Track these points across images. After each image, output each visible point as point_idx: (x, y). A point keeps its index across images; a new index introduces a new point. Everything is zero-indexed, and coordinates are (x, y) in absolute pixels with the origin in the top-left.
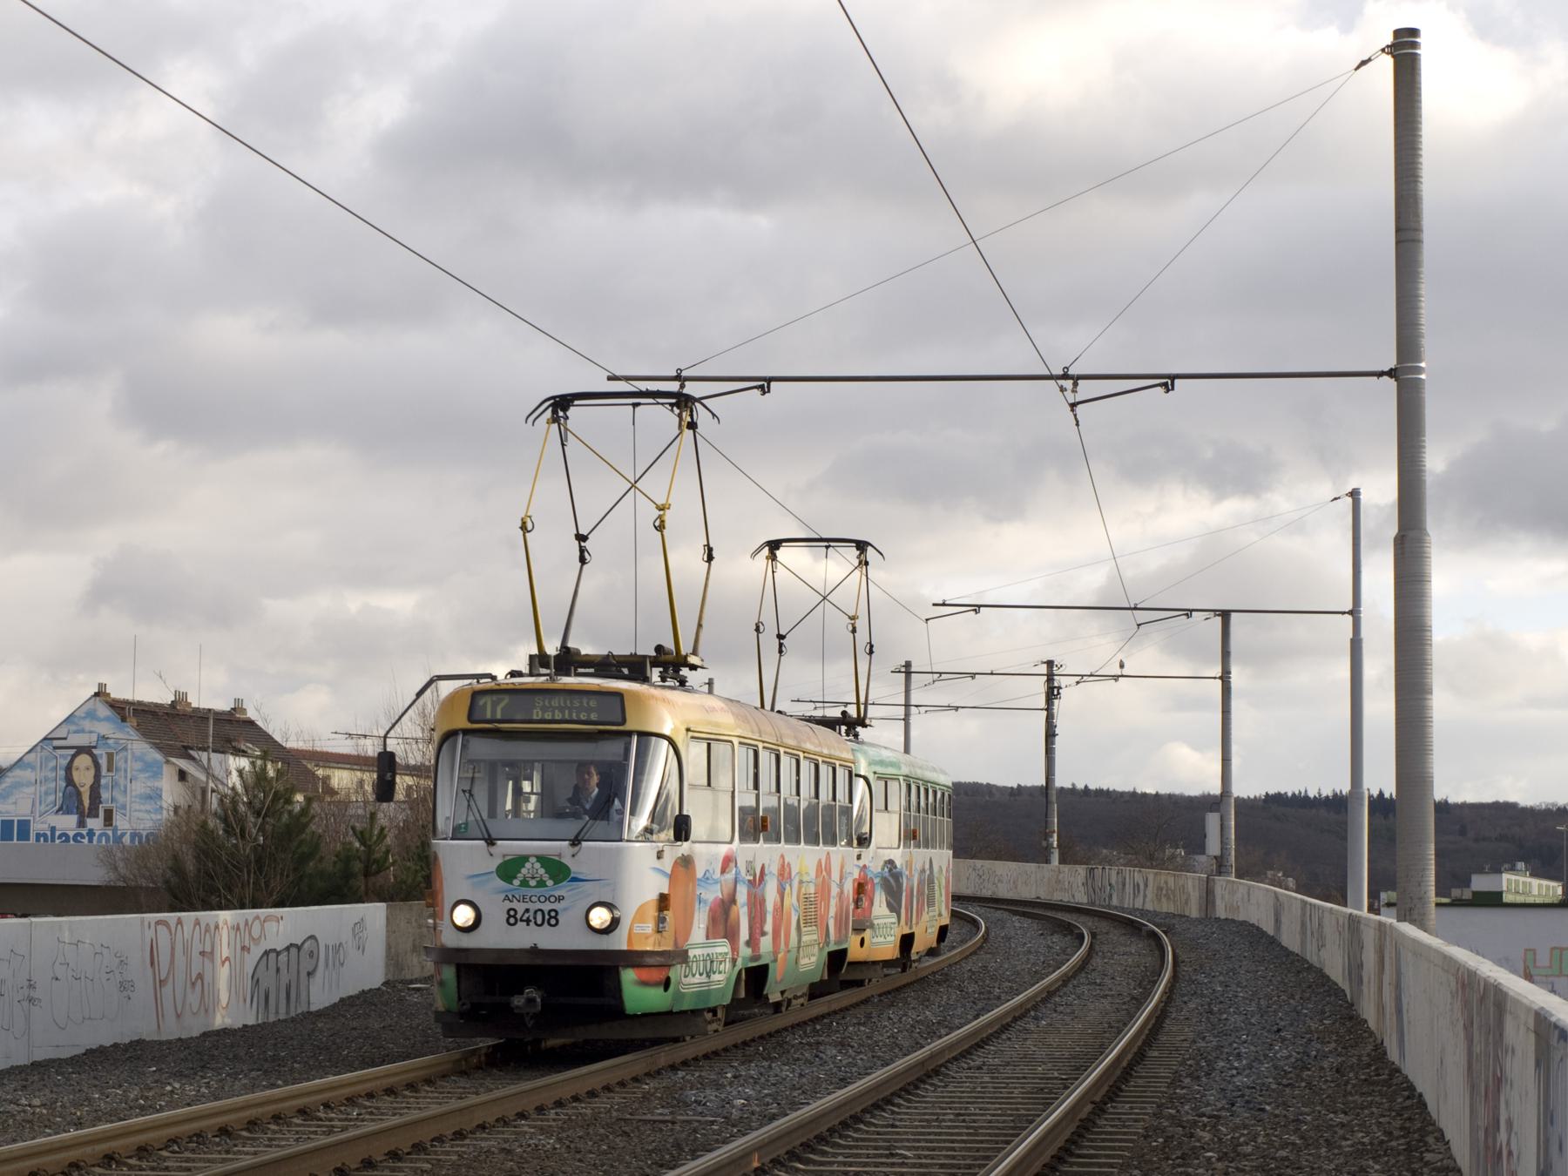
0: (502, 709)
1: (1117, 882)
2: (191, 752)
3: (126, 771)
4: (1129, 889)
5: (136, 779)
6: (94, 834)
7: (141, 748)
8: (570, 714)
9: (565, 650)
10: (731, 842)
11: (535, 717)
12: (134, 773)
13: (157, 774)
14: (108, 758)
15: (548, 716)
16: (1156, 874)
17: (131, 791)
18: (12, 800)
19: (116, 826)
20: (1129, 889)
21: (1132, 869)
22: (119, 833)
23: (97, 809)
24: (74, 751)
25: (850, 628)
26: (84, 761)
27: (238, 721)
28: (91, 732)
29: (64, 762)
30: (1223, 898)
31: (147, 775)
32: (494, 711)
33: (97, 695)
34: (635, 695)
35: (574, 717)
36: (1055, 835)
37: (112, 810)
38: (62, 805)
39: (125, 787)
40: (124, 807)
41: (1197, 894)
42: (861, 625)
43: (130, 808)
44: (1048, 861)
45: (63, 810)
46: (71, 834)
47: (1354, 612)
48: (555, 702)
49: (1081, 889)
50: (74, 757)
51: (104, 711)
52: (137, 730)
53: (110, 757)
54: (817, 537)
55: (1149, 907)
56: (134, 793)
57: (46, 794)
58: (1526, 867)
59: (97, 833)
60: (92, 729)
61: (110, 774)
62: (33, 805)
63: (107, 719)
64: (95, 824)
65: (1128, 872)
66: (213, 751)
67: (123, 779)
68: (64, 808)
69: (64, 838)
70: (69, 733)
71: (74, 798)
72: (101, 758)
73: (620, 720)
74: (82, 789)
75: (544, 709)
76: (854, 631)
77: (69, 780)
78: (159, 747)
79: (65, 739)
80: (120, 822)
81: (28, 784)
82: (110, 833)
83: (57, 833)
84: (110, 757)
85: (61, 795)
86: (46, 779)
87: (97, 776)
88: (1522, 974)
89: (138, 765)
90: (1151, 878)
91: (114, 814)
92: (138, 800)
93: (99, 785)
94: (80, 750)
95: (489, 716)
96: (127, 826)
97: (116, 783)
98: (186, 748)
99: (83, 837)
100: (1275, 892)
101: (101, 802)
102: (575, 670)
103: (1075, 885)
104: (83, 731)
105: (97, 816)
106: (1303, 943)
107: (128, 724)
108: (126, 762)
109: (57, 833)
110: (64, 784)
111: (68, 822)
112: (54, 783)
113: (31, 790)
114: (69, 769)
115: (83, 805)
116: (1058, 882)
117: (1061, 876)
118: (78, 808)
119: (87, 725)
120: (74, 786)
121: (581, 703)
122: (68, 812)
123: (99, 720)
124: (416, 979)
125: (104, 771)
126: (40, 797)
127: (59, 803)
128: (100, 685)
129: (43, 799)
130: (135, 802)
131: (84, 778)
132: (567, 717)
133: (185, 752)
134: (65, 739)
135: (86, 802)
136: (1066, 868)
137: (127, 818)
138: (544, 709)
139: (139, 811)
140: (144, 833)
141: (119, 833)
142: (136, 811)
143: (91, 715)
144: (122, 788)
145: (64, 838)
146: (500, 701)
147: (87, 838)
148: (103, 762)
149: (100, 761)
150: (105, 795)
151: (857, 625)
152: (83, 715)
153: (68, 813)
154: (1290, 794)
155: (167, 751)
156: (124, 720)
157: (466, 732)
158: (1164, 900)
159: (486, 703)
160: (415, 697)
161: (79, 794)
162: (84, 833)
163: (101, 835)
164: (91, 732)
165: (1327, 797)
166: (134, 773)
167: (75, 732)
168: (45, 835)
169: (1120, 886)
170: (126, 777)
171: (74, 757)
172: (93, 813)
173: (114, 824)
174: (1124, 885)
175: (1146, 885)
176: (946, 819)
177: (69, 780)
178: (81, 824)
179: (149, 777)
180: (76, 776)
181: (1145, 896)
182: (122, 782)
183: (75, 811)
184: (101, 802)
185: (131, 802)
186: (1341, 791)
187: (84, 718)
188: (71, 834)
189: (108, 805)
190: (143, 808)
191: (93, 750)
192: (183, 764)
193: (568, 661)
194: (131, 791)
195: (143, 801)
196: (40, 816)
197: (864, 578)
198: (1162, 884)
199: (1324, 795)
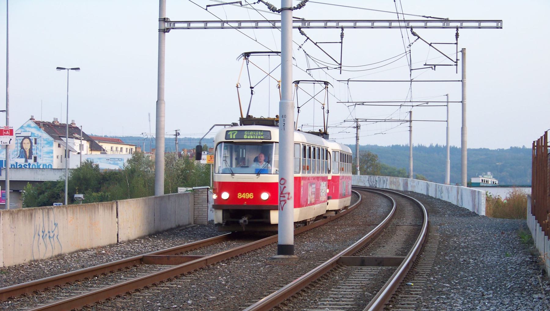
0: (236, 135)
1: (378, 180)
2: (62, 138)
3: (41, 144)
4: (382, 182)
5: (44, 147)
6: (30, 165)
7: (45, 136)
8: (255, 137)
9: (248, 116)
10: (339, 173)
11: (245, 138)
12: (44, 145)
13: (51, 144)
14: (35, 140)
15: (249, 137)
16: (390, 178)
17: (43, 151)
19: (38, 162)
20: (382, 182)
21: (383, 176)
22: (39, 164)
23: (31, 156)
24: (23, 138)
25: (322, 107)
26: (27, 141)
27: (74, 127)
28: (29, 131)
29: (20, 141)
30: (410, 184)
31: (48, 145)
32: (233, 136)
33: (31, 119)
34: (359, 149)
35: (257, 138)
36: (359, 167)
37: (36, 157)
38: (19, 155)
39: (41, 150)
40: (40, 156)
41: (402, 183)
42: (326, 107)
43: (43, 156)
45: (20, 157)
46: (23, 165)
48: (251, 133)
49: (368, 182)
50: (23, 140)
51: (33, 125)
52: (45, 131)
53: (36, 140)
54: (315, 80)
55: (388, 187)
56: (44, 151)
58: (491, 174)
59: (32, 164)
60: (29, 130)
61: (36, 145)
63: (35, 127)
64: (31, 161)
65: (381, 177)
66: (69, 138)
67: (40, 147)
68: (20, 156)
69: (20, 166)
70: (21, 132)
71: (24, 153)
72: (33, 140)
73: (270, 139)
74: (26, 150)
75: (247, 135)
76: (324, 108)
77: (22, 147)
78: (52, 136)
79: (20, 134)
80: (39, 160)
82: (36, 164)
83: (18, 164)
84: (36, 140)
85: (19, 152)
87: (31, 146)
88: (295, 234)
89: (45, 142)
91: (37, 158)
92: (45, 153)
93: (32, 149)
94: (25, 137)
95: (231, 137)
97: (38, 148)
99: (27, 165)
100: (427, 182)
101: (33, 154)
103: (365, 181)
104: (26, 131)
105: (31, 159)
106: (436, 193)
107: (42, 129)
108: (41, 141)
109: (18, 164)
110: (20, 148)
111: (22, 161)
112: (17, 148)
114: (22, 143)
115: (27, 155)
116: (360, 180)
117: (361, 178)
118: (25, 156)
119: (28, 129)
120: (24, 149)
121: (258, 133)
122: (22, 157)
123: (32, 128)
125: (34, 144)
126: (12, 153)
127: (18, 154)
129: (13, 153)
130: (44, 154)
131: (27, 146)
132: (254, 138)
133: (59, 138)
134: (20, 134)
135: (28, 154)
136: (362, 176)
137: (42, 159)
138: (247, 135)
139: (46, 157)
140: (47, 164)
141: (39, 164)
142: (44, 157)
143: (29, 126)
144: (40, 150)
145: (20, 166)
146: (235, 133)
147: (28, 166)
148: (33, 141)
149: (32, 141)
150: (34, 152)
151: (324, 107)
152: (26, 126)
153: (22, 158)
154: (401, 146)
155: (55, 138)
156: (40, 128)
157: (225, 142)
158: (392, 185)
159: (230, 134)
160: (209, 130)
161: (25, 152)
162: (27, 164)
163: (33, 165)
164: (29, 131)
166: (44, 145)
167: (24, 131)
168: (14, 165)
169: (379, 181)
170: (41, 146)
171: (23, 140)
172: (30, 157)
173: (37, 161)
174: (380, 181)
175: (387, 181)
176: (348, 163)
177: (22, 147)
178: (26, 161)
179: (48, 146)
180: (24, 146)
181: (386, 184)
182: (40, 148)
183: (24, 157)
184: (33, 154)
185: (43, 154)
186: (421, 145)
187: (26, 127)
188: (23, 165)
189: (35, 155)
190: (47, 156)
191: (30, 138)
192: (59, 142)
193: (248, 120)
194: (43, 151)
195: (47, 154)
196: (12, 159)
197: (327, 91)
198: (392, 180)
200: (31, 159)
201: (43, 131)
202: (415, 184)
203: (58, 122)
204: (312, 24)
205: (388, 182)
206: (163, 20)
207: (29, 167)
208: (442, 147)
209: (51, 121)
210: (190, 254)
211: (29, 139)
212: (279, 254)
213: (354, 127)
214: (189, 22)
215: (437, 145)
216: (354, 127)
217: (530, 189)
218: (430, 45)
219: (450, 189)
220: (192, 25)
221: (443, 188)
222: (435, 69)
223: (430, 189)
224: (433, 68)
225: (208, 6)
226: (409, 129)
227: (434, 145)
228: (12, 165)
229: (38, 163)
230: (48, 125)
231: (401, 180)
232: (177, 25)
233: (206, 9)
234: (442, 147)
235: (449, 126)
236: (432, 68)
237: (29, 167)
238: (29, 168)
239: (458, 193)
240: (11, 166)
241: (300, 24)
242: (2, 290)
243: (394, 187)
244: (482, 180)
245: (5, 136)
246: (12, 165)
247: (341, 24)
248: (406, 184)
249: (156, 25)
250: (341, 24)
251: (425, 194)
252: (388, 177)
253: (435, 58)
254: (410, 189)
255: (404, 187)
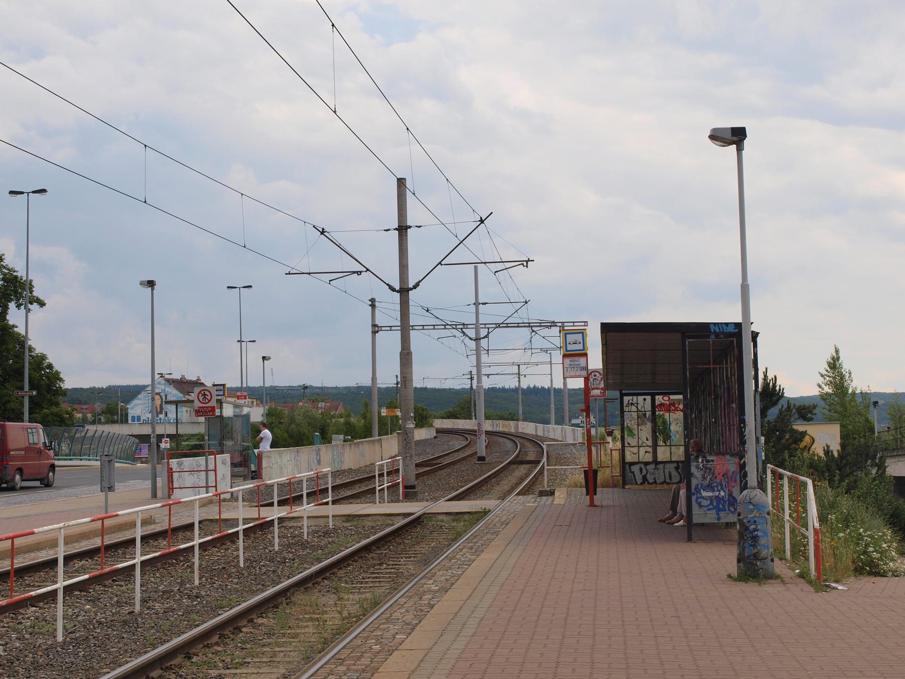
2: (190, 394)
4: (495, 425)
18: (134, 409)
20: (495, 425)
28: (159, 388)
44: (472, 419)
47: (551, 374)
51: (163, 382)
55: (501, 430)
57: (146, 407)
62: (142, 411)
81: (140, 405)
82: (166, 419)
86: (146, 403)
90: (501, 423)
96: (172, 416)
98: (189, 392)
102: (570, 420)
105: (162, 414)
106: (544, 433)
113: (141, 406)
124: (621, 413)
128: (198, 377)
135: (159, 410)
164: (159, 388)
165: (513, 389)
168: (146, 420)
199: (511, 387)
200: (162, 414)
201: (173, 388)
202: (525, 426)
203: (185, 379)
204: (469, 326)
205: (501, 425)
206: (374, 326)
207: (160, 421)
208: (540, 387)
209: (179, 378)
210: (435, 462)
211: (160, 395)
212: (478, 461)
213: (469, 379)
214: (391, 327)
215: (535, 386)
216: (469, 379)
217: (246, 386)
218: (544, 338)
219: (555, 429)
220: (393, 328)
221: (550, 429)
222: (527, 266)
223: (538, 429)
224: (525, 265)
225: (330, 281)
226: (518, 379)
227: (532, 386)
228: (143, 420)
229: (168, 418)
230: (177, 382)
231: (512, 423)
232: (383, 328)
233: (330, 284)
234: (540, 387)
235: (553, 378)
236: (523, 264)
237: (160, 421)
238: (160, 422)
239: (562, 432)
240: (143, 421)
241: (461, 327)
242: (2, 572)
243: (506, 430)
244: (581, 421)
245: (241, 400)
246: (143, 420)
247: (487, 326)
248: (517, 427)
249: (370, 329)
250: (487, 326)
251: (534, 434)
252: (501, 421)
253: (547, 345)
254: (520, 431)
255: (515, 428)
